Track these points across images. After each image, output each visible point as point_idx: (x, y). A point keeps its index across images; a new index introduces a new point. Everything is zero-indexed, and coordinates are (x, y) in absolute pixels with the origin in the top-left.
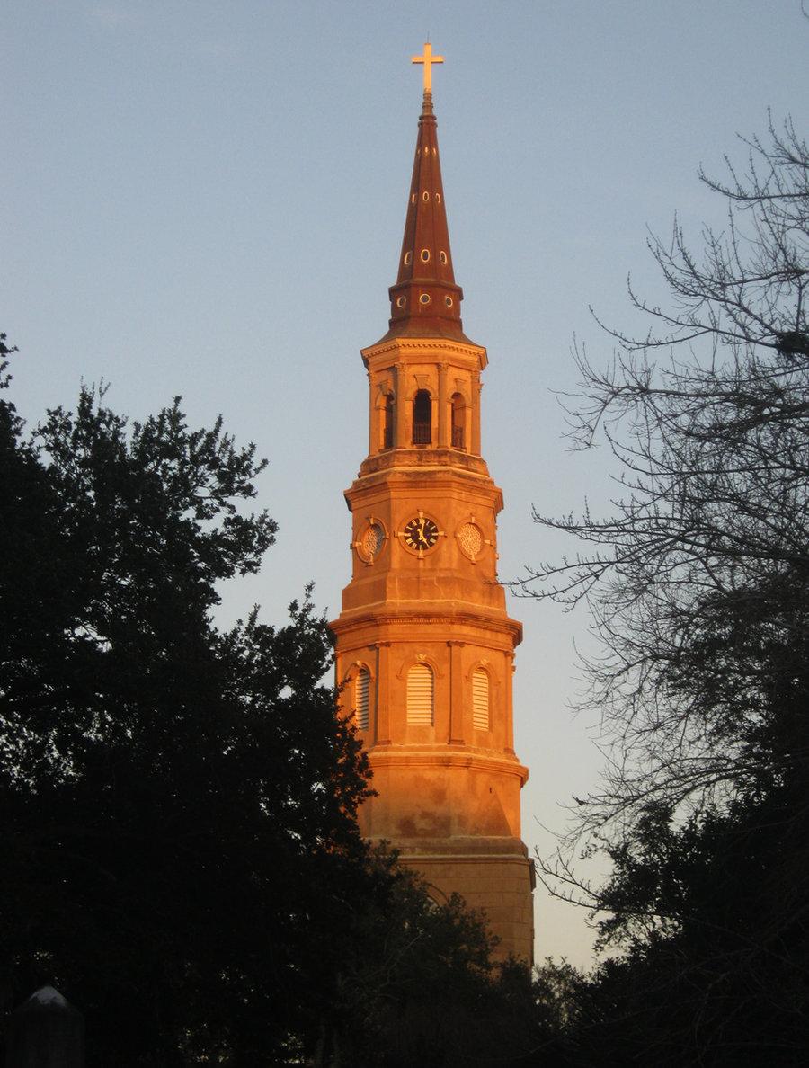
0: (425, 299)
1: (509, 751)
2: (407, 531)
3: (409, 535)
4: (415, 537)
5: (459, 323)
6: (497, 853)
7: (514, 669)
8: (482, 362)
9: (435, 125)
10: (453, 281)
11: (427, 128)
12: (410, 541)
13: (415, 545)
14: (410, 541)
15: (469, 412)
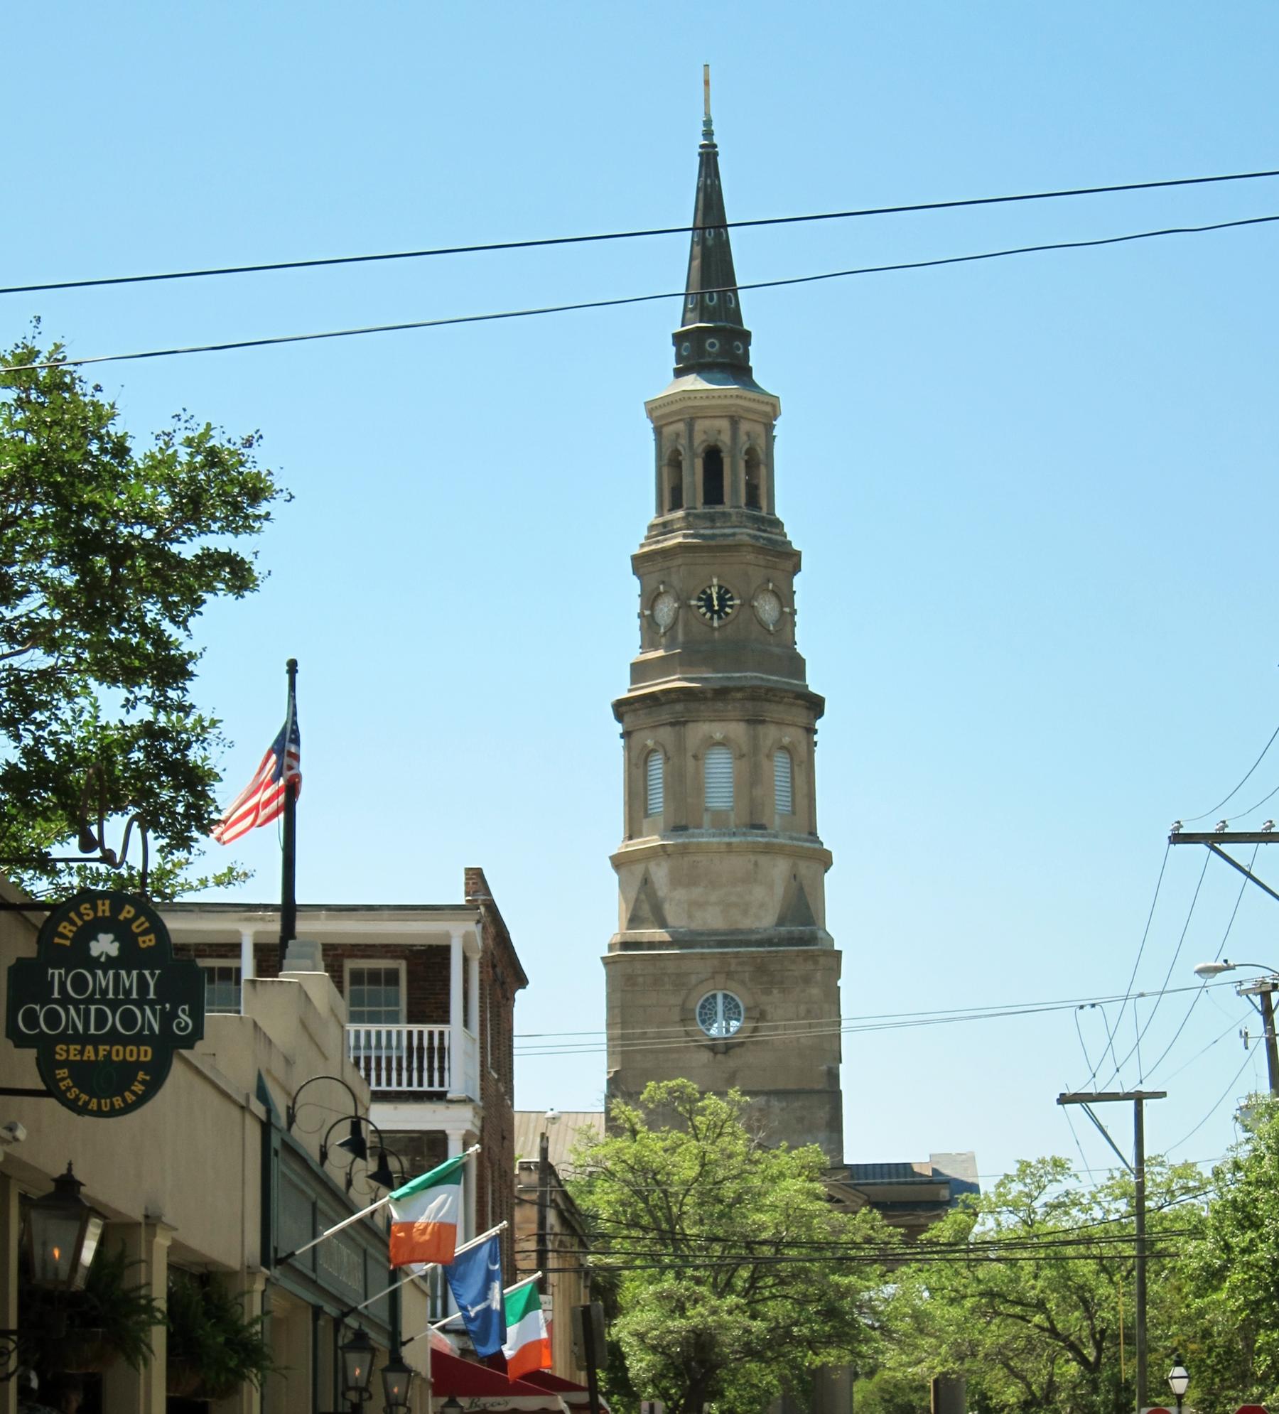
0: (712, 345)
1: (813, 833)
2: (700, 599)
3: (702, 603)
4: (709, 606)
5: (750, 369)
6: (702, 954)
7: (816, 744)
8: (775, 413)
9: (716, 154)
10: (741, 324)
11: (709, 158)
12: (703, 610)
13: (708, 615)
14: (703, 610)
15: (763, 470)
